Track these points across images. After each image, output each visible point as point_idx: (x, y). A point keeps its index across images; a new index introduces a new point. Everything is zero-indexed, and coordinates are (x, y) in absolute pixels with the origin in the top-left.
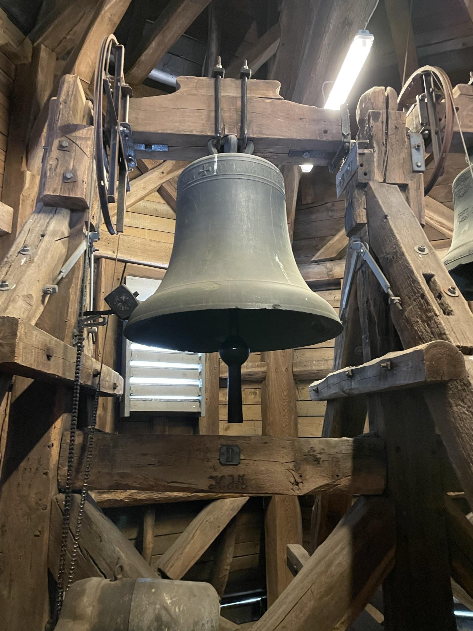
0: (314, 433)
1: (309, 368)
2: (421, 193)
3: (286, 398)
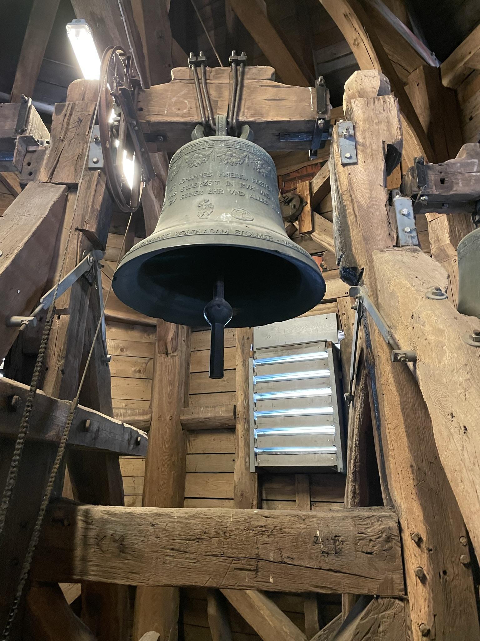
0: (201, 493)
1: (196, 416)
2: (90, 193)
3: (168, 451)
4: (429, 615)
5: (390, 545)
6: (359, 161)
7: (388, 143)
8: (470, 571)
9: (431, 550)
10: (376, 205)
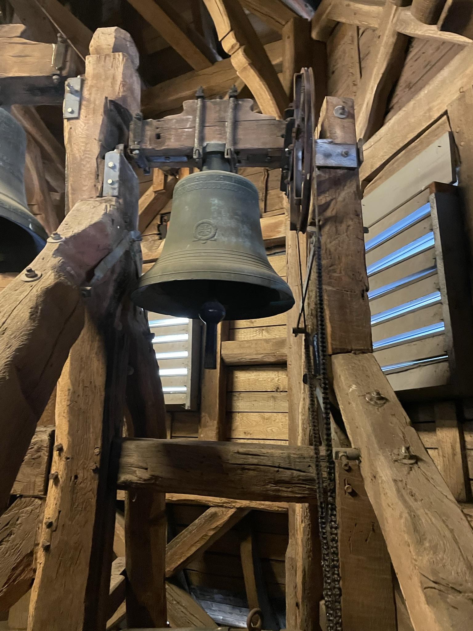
4: (55, 511)
5: (39, 454)
6: (81, 116)
7: (111, 99)
8: (97, 476)
9: (68, 458)
10: (89, 158)
